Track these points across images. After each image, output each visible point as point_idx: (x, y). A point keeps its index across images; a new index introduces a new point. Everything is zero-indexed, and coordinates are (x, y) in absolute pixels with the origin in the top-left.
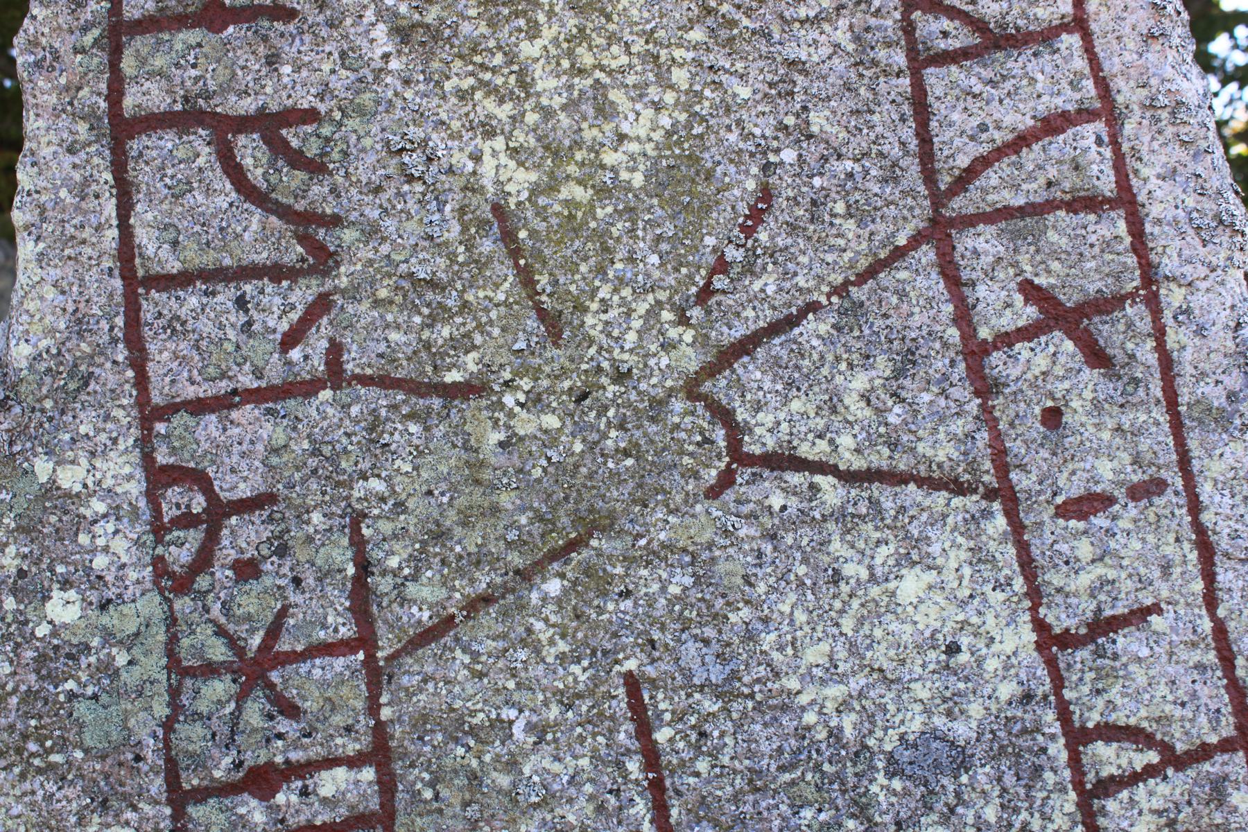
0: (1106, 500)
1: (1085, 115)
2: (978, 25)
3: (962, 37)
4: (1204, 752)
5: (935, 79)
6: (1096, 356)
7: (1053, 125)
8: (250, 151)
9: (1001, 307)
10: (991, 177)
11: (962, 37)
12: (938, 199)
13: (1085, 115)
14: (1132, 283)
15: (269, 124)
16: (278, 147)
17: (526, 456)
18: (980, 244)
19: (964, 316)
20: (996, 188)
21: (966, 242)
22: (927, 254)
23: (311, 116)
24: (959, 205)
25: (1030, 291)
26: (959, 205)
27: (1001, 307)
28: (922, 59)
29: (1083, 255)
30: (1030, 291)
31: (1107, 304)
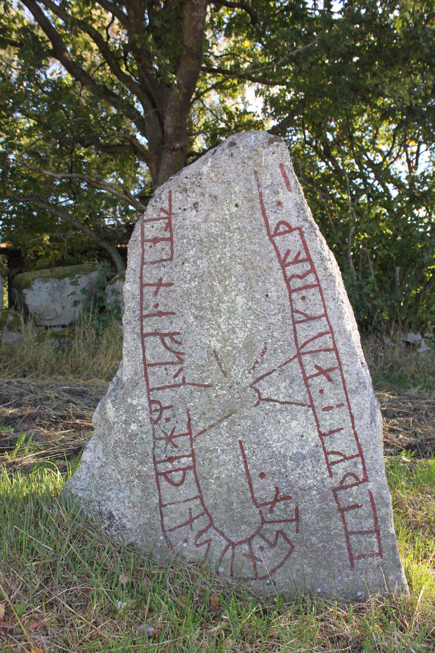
2: (306, 315)
3: (303, 318)
5: (297, 325)
8: (167, 340)
9: (311, 370)
12: (298, 349)
16: (173, 339)
18: (307, 358)
19: (303, 372)
20: (310, 347)
22: (296, 360)
23: (179, 333)
24: (302, 350)
26: (302, 350)
27: (311, 370)
28: (295, 322)
29: (327, 360)
30: (316, 367)
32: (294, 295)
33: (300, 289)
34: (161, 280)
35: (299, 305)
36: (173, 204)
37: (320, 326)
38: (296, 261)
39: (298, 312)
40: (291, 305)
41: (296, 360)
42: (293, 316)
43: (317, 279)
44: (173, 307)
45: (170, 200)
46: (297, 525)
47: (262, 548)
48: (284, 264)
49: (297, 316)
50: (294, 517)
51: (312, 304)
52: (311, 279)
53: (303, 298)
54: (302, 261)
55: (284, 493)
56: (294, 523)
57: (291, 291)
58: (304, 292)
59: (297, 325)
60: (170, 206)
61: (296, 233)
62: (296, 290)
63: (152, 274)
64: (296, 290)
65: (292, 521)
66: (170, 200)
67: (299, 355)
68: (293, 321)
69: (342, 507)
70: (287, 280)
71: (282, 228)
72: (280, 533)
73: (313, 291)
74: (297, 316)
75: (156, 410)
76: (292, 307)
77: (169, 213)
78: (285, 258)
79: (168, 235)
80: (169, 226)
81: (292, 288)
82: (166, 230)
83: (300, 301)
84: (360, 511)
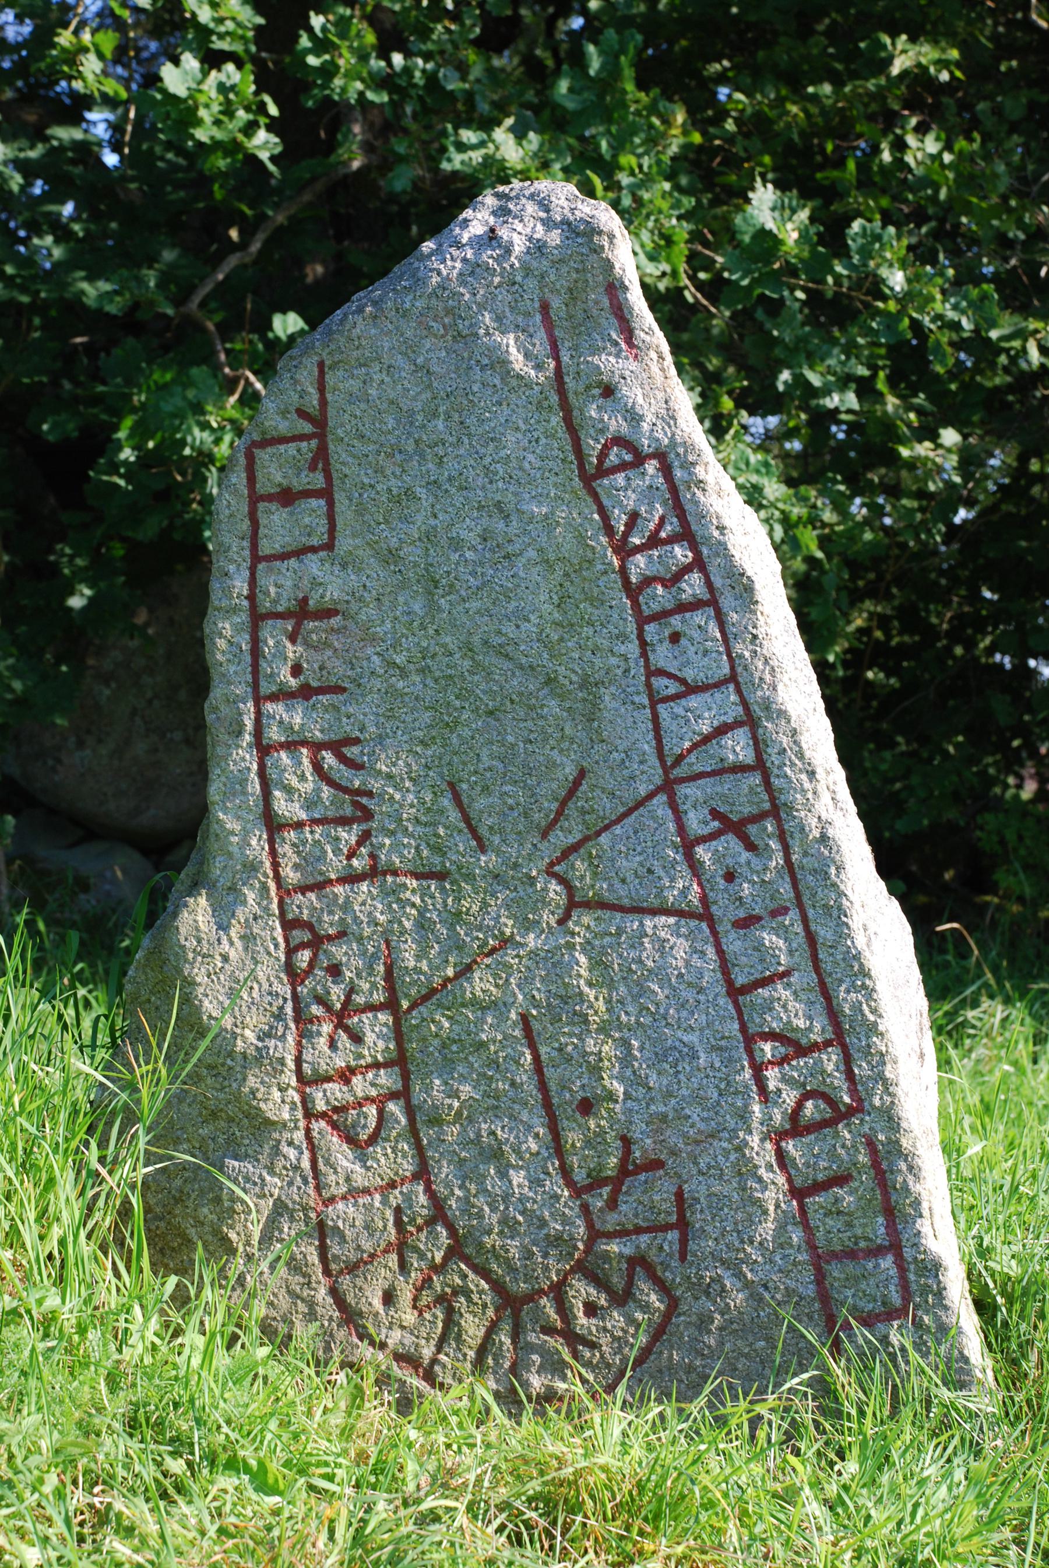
0: (759, 918)
1: (737, 724)
2: (683, 681)
3: (673, 688)
4: (815, 1047)
5: (661, 708)
6: (751, 847)
7: (722, 730)
8: (329, 759)
9: (696, 822)
10: (692, 758)
11: (673, 688)
12: (666, 770)
13: (737, 724)
14: (767, 806)
15: (336, 747)
16: (342, 759)
17: (386, 600)
18: (688, 791)
19: (681, 829)
20: (695, 763)
21: (685, 790)
22: (661, 798)
23: (357, 741)
24: (677, 772)
25: (715, 814)
26: (677, 772)
27: (696, 822)
28: (655, 700)
29: (744, 795)
30: (715, 814)
31: (757, 818)
32: (650, 628)
33: (665, 614)
34: (305, 600)
35: (662, 656)
36: (329, 397)
37: (721, 706)
38: (654, 541)
39: (662, 673)
40: (644, 654)
41: (661, 798)
42: (648, 685)
43: (709, 584)
44: (339, 671)
45: (322, 389)
46: (684, 1242)
47: (591, 1309)
48: (624, 551)
49: (665, 686)
50: (674, 1219)
51: (700, 656)
52: (693, 585)
53: (675, 638)
54: (671, 540)
55: (645, 1151)
56: (673, 1235)
57: (642, 621)
58: (676, 621)
59: (661, 708)
60: (323, 402)
61: (651, 467)
62: (656, 617)
63: (279, 586)
64: (656, 617)
65: (666, 1228)
66: (322, 389)
67: (668, 787)
68: (651, 696)
69: (798, 1182)
70: (633, 592)
71: (614, 457)
72: (638, 1262)
73: (699, 618)
74: (659, 683)
75: (303, 946)
76: (647, 660)
77: (320, 422)
78: (626, 534)
79: (318, 480)
80: (321, 458)
81: (647, 612)
82: (313, 468)
83: (666, 644)
84: (327, 363)
